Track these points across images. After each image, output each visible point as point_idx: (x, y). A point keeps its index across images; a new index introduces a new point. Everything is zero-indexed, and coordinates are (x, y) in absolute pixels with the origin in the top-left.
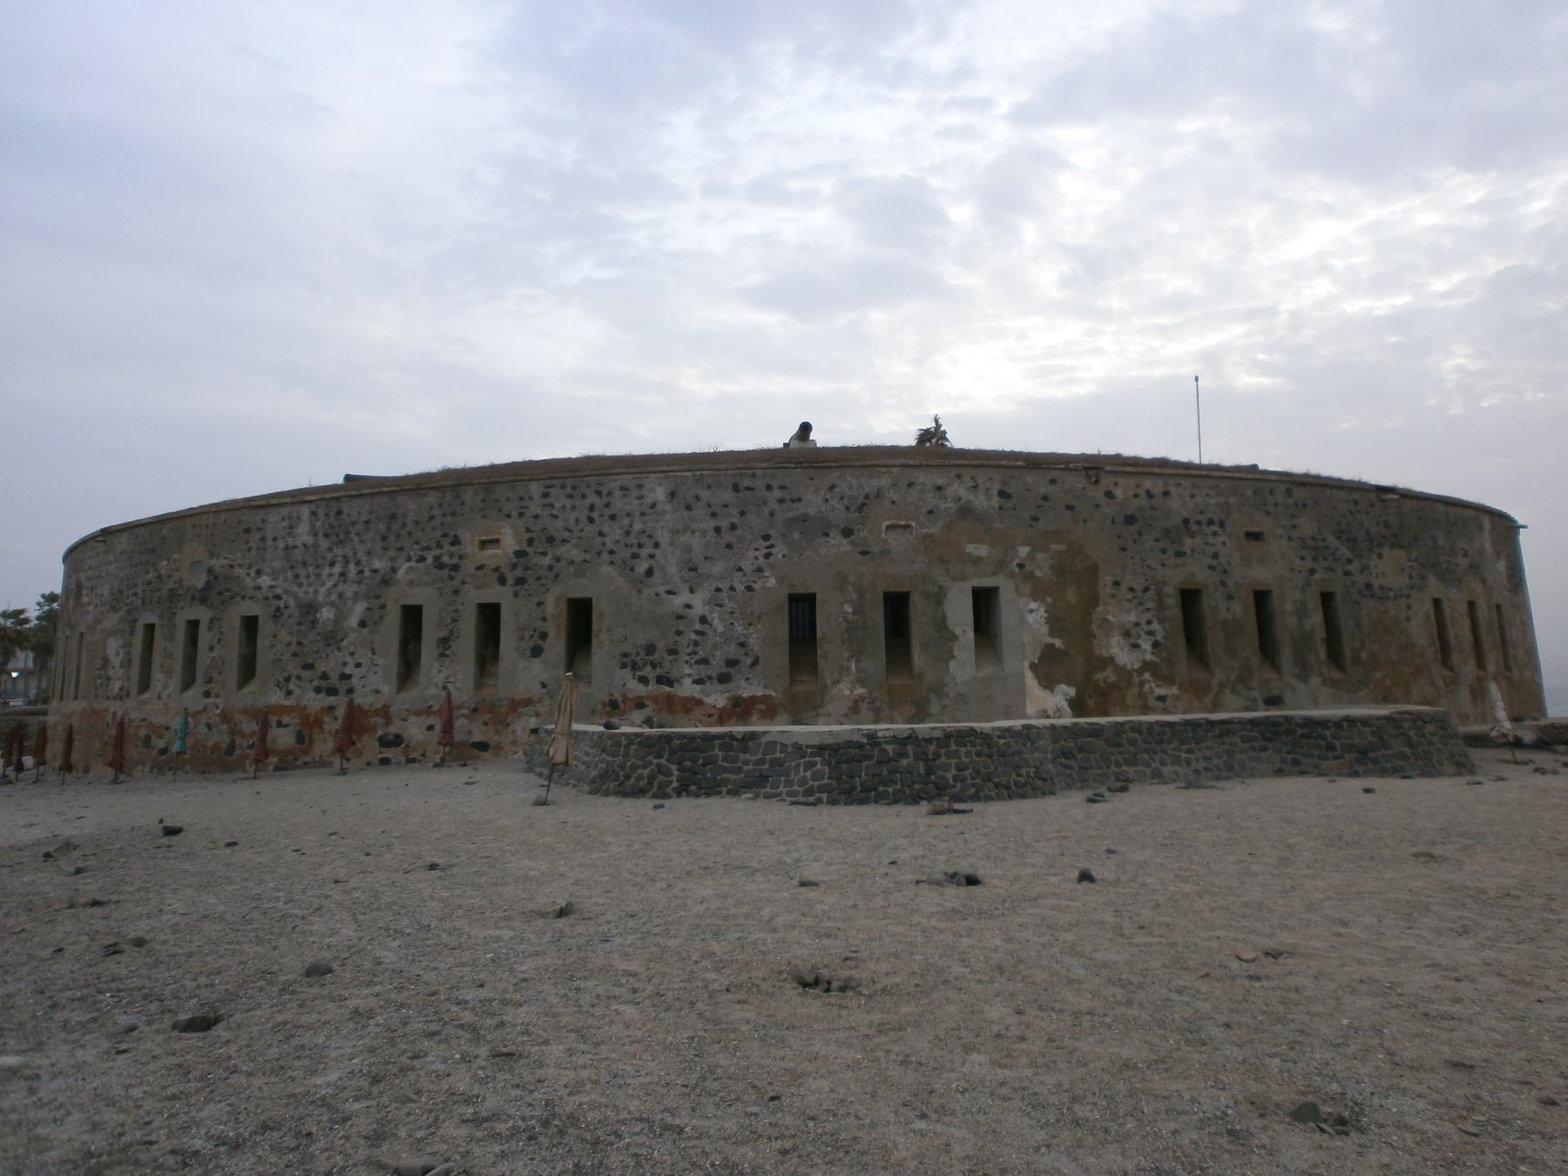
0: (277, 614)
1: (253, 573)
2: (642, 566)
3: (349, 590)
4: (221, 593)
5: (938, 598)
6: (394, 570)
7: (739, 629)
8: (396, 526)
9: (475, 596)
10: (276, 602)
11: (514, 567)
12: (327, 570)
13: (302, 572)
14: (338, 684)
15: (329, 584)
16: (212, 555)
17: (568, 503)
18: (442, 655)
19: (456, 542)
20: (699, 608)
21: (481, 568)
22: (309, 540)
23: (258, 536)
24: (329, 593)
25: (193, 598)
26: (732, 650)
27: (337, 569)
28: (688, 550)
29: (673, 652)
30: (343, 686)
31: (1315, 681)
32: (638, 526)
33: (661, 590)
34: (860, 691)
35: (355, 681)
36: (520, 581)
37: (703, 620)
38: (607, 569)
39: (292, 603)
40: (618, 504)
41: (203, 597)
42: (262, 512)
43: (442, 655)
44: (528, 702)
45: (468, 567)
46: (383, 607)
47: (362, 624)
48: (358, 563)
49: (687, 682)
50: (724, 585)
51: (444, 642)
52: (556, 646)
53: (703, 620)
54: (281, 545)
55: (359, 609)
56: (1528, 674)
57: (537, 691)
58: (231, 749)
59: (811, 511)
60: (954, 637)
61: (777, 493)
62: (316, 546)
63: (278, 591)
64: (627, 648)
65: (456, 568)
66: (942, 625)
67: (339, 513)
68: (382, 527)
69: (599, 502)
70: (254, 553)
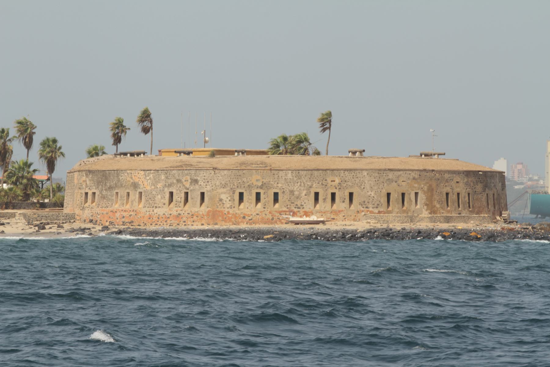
0: (283, 192)
1: (276, 183)
2: (362, 187)
3: (302, 188)
4: (267, 187)
5: (410, 194)
6: (312, 185)
7: (379, 199)
8: (312, 176)
9: (330, 191)
10: (283, 190)
11: (338, 186)
12: (296, 184)
13: (290, 184)
14: (300, 207)
15: (297, 187)
16: (263, 179)
17: (349, 175)
18: (324, 202)
19: (326, 180)
20: (373, 195)
21: (331, 186)
22: (292, 178)
23: (277, 176)
24: (297, 188)
25: (257, 187)
26: (378, 202)
27: (299, 184)
28: (371, 184)
29: (368, 202)
30: (302, 207)
31: (466, 210)
32: (362, 180)
33: (366, 191)
34: (398, 210)
35: (304, 206)
36: (340, 189)
37: (373, 197)
38: (356, 187)
39: (288, 190)
40: (358, 175)
41: (261, 187)
42: (278, 171)
43: (324, 202)
44: (342, 211)
45: (329, 185)
46: (310, 192)
47: (306, 195)
48: (304, 183)
49: (371, 208)
50: (377, 191)
51: (324, 199)
52: (347, 200)
53: (373, 197)
54: (284, 178)
55: (304, 192)
56: (46, 242)
57: (344, 209)
58: (273, 219)
59: (390, 178)
60: (412, 201)
61: (385, 174)
62: (293, 179)
63: (284, 187)
64: (360, 202)
65: (326, 185)
66: (410, 199)
67: (299, 173)
68: (309, 176)
69: (355, 175)
70: (276, 179)
